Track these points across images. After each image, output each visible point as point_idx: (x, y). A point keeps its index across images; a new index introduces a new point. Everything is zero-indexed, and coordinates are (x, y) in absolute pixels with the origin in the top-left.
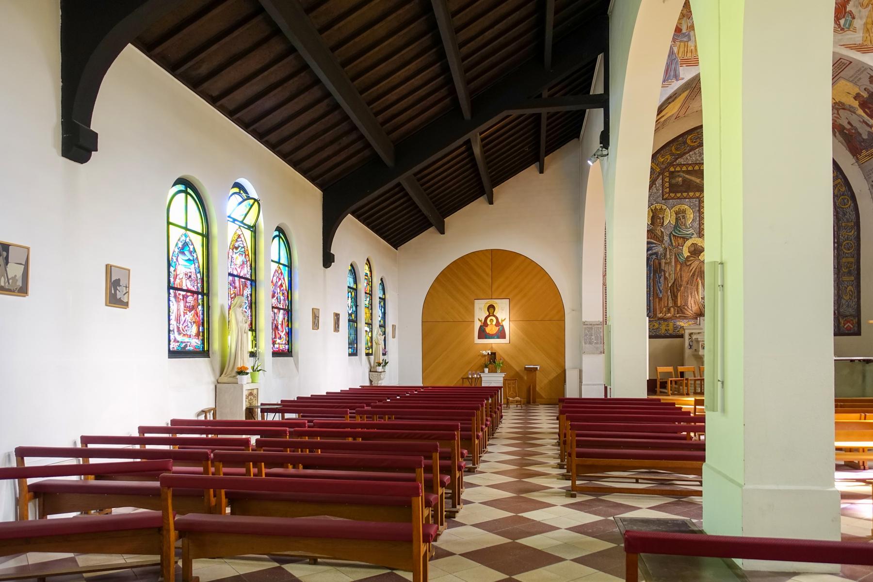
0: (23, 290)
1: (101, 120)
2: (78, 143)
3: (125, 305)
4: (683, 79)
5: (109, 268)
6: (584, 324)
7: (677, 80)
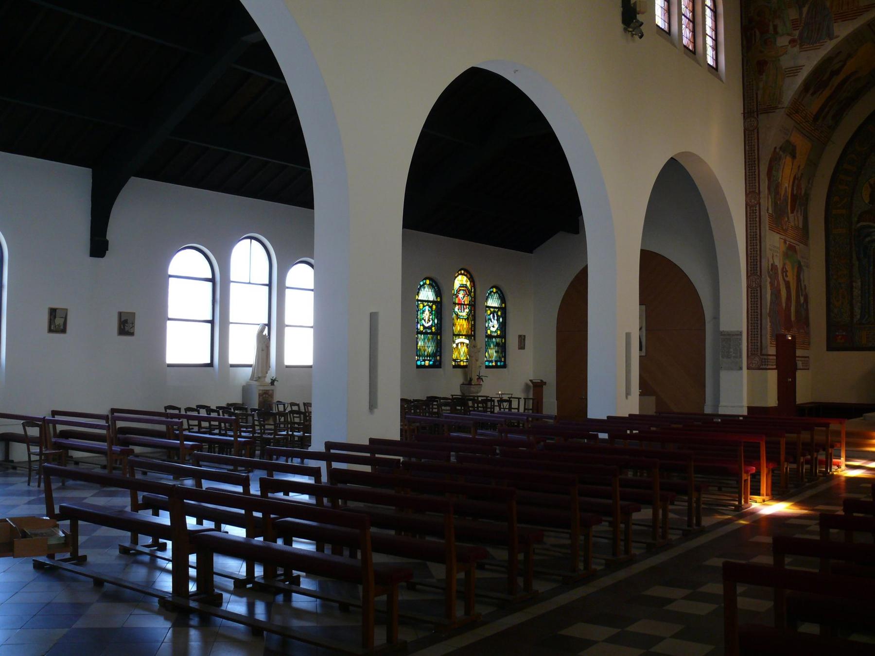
0: (63, 331)
1: (112, 235)
2: (99, 247)
3: (132, 334)
4: (837, 37)
5: (120, 314)
6: (722, 334)
7: (831, 39)
